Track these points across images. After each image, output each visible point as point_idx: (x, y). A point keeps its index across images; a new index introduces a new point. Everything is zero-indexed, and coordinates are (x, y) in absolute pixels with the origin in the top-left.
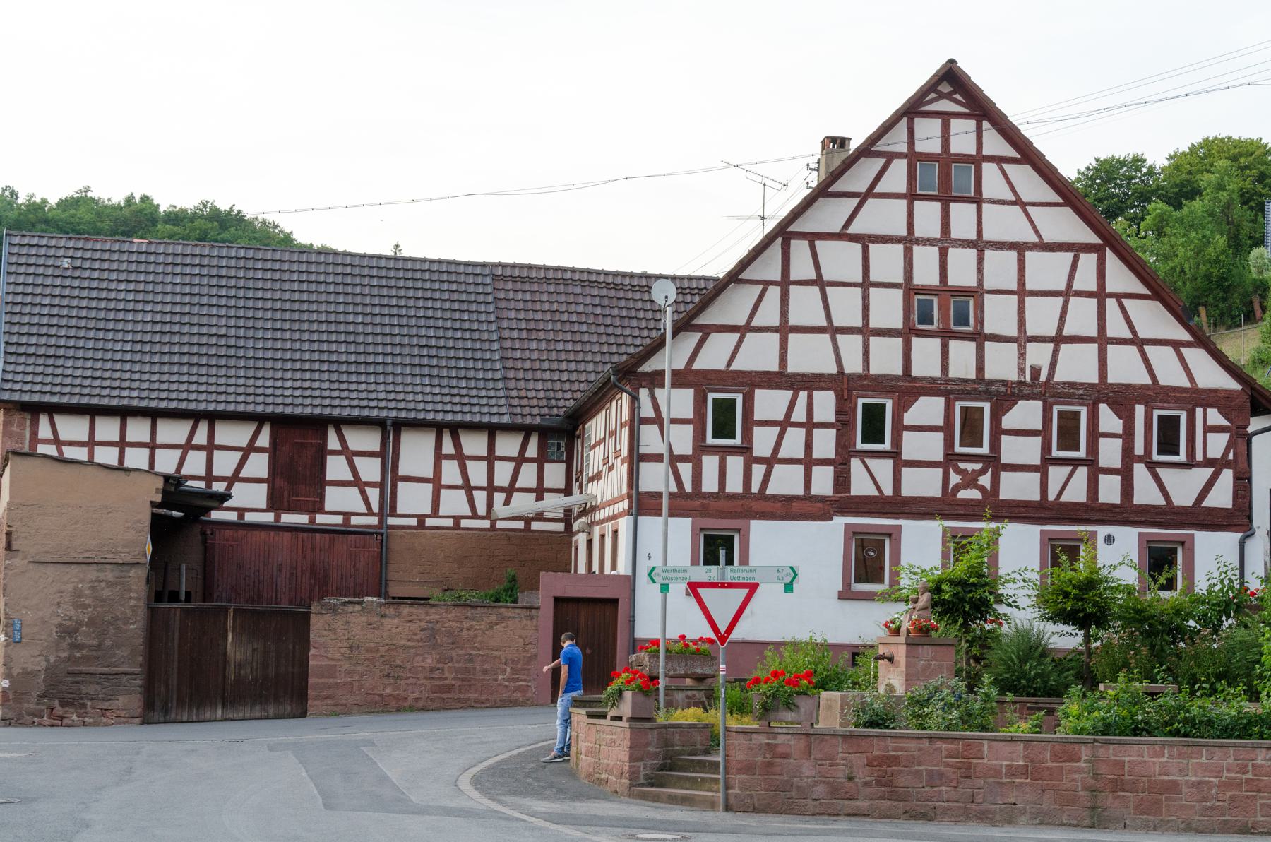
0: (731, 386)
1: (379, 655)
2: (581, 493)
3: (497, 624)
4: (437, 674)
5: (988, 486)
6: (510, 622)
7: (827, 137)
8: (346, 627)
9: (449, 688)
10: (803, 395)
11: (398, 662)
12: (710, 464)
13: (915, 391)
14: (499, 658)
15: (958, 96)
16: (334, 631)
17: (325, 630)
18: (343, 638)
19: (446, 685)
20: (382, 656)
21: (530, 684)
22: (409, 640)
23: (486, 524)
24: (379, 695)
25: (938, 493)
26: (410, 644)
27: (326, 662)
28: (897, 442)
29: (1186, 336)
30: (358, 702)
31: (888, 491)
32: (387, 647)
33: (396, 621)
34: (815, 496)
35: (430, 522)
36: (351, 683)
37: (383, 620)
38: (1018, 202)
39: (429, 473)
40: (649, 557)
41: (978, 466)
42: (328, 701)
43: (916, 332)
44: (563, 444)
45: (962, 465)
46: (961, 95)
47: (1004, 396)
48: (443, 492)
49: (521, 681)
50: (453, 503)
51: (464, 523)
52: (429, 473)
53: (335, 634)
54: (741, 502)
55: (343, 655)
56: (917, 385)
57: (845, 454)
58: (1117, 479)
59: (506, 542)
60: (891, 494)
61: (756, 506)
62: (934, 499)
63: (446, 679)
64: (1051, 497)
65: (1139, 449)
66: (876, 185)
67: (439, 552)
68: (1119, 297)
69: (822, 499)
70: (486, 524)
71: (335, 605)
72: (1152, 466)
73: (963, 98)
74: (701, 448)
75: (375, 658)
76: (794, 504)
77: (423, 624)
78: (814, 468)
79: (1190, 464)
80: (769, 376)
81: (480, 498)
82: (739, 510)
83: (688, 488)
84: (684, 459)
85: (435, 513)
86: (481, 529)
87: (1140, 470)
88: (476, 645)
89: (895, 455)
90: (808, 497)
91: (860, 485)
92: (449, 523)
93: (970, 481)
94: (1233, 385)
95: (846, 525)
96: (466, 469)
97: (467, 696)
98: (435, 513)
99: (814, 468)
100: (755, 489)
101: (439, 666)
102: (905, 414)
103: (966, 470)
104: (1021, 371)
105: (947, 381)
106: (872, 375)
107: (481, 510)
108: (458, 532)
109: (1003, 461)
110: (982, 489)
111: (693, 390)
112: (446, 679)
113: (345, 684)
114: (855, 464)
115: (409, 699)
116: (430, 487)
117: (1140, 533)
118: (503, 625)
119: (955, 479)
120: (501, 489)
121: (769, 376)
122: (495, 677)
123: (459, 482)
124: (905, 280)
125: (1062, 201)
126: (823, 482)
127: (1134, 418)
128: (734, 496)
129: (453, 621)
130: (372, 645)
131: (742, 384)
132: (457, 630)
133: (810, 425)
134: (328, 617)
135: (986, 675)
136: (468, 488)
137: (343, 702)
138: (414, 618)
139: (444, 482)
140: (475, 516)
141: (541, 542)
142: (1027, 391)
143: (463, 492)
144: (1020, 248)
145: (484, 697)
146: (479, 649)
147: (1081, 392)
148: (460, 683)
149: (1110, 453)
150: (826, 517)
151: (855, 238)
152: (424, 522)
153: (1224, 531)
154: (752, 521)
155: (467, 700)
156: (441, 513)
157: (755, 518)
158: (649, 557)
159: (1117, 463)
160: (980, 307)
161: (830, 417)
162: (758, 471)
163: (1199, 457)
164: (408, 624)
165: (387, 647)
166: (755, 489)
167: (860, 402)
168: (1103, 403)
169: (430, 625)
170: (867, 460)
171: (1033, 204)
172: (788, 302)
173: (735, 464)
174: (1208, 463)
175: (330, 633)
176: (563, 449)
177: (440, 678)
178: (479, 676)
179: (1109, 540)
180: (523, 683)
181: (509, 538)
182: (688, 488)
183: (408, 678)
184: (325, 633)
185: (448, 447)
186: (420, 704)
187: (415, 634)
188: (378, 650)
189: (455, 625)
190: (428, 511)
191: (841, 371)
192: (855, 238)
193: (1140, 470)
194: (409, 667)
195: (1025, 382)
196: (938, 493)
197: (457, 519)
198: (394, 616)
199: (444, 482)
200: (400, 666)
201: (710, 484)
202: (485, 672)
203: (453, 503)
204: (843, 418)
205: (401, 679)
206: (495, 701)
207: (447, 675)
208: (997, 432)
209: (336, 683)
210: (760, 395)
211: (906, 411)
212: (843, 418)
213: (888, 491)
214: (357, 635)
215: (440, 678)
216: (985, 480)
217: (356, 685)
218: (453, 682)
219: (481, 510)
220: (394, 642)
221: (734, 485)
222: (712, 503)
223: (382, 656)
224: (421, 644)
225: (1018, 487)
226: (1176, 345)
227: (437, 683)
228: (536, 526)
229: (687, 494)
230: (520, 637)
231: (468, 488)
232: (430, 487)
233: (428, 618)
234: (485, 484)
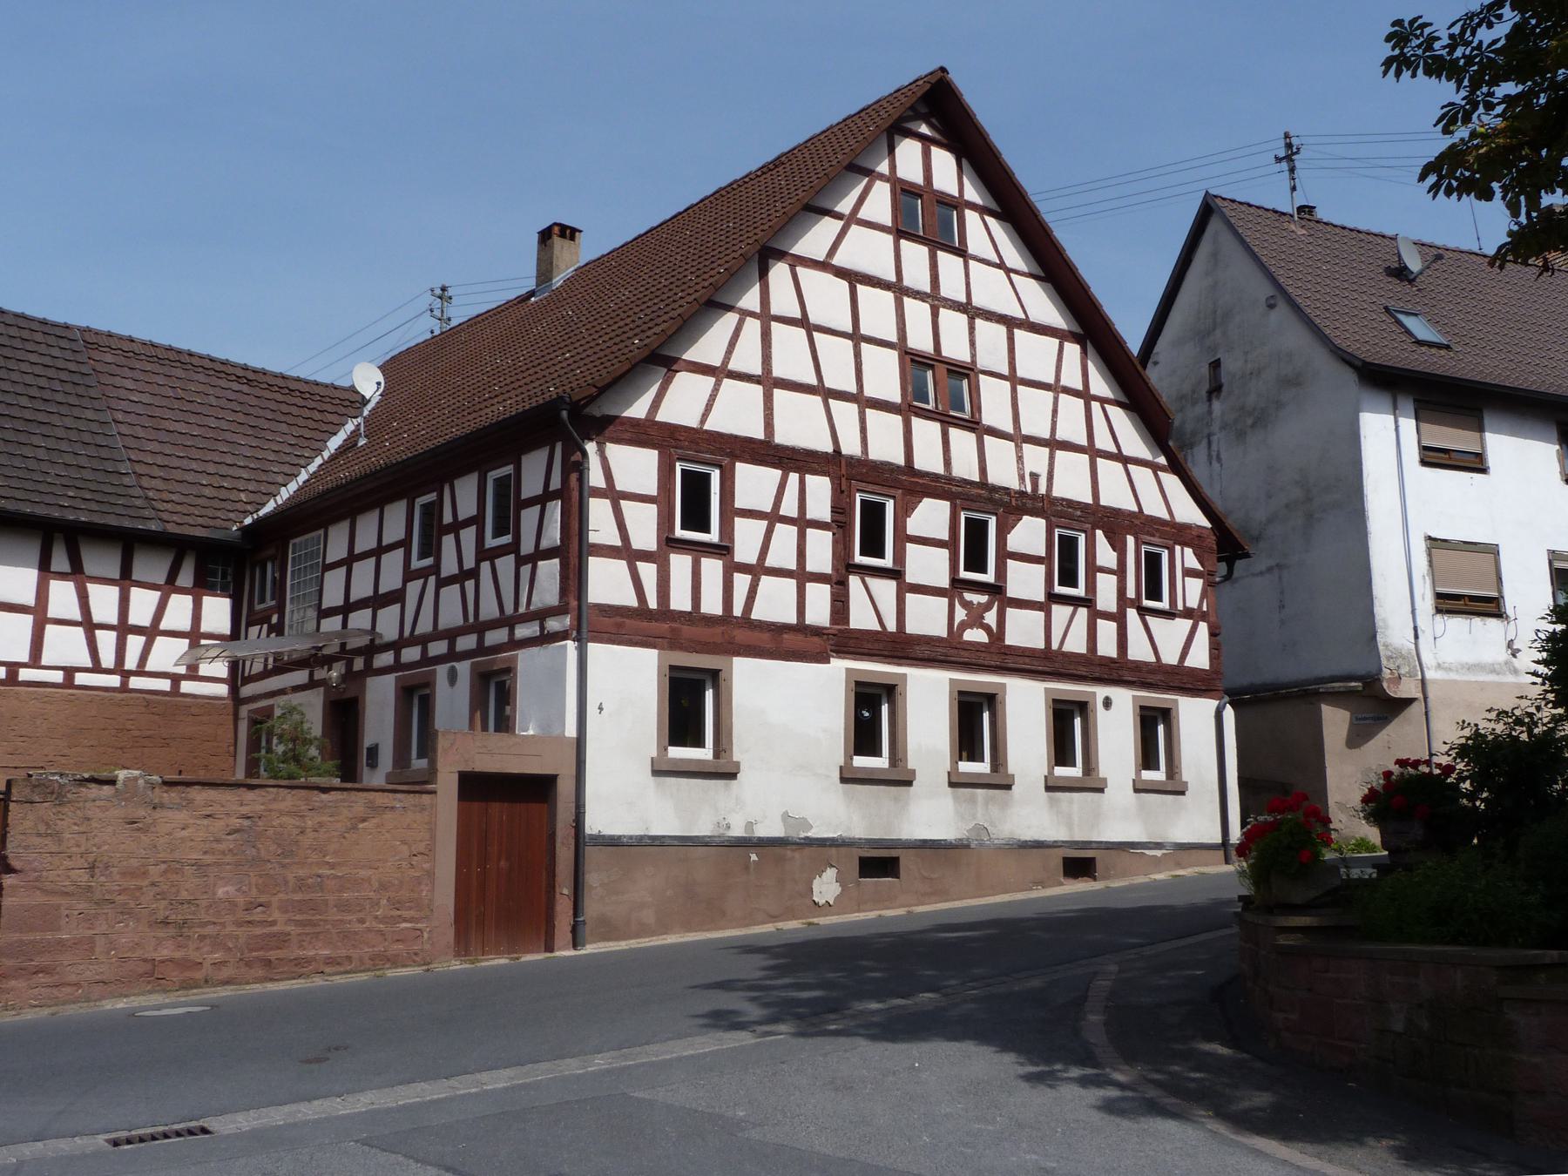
0: (706, 453)
1: (146, 882)
2: (246, 639)
3: (364, 820)
4: (257, 914)
5: (994, 626)
6: (388, 816)
7: (555, 224)
8: (82, 829)
9: (282, 940)
10: (794, 478)
11: (184, 895)
12: (680, 564)
13: (918, 489)
14: (369, 880)
15: (934, 120)
16: (57, 836)
17: (39, 835)
18: (74, 849)
19: (274, 935)
20: (153, 884)
21: (419, 926)
22: (205, 853)
23: (114, 681)
24: (145, 960)
25: (943, 632)
26: (208, 859)
27: (39, 898)
28: (900, 556)
29: (1162, 460)
30: (104, 977)
31: (891, 626)
32: (163, 867)
33: (181, 816)
34: (809, 626)
35: (25, 674)
36: (91, 941)
37: (158, 814)
38: (1001, 265)
39: (29, 599)
40: (601, 709)
41: (984, 599)
42: (41, 978)
43: (916, 410)
44: (230, 570)
45: (968, 596)
46: (937, 119)
47: (1014, 505)
48: (49, 629)
49: (405, 920)
50: (65, 646)
51: (81, 679)
52: (29, 599)
53: (60, 841)
54: (719, 630)
55: (74, 883)
56: (921, 481)
57: (844, 569)
58: (1113, 625)
59: (143, 710)
60: (895, 631)
61: (741, 636)
62: (939, 639)
63: (273, 923)
64: (1055, 646)
65: (1131, 593)
66: (859, 209)
67: (38, 722)
68: (1103, 401)
69: (817, 631)
70: (114, 681)
71: (61, 786)
72: (1143, 612)
73: (939, 123)
74: (670, 543)
75: (141, 888)
76: (785, 636)
77: (236, 822)
78: (807, 584)
79: (1169, 615)
80: (753, 446)
81: (106, 640)
82: (719, 640)
83: (653, 603)
84: (646, 556)
85: (35, 661)
86: (106, 689)
87: (1132, 614)
88: (327, 859)
89: (896, 574)
90: (801, 628)
91: (861, 618)
92: (58, 677)
93: (976, 620)
94: (1203, 521)
95: (848, 671)
96: (87, 597)
97: (312, 953)
98: (35, 661)
99: (807, 584)
100: (738, 611)
101: (262, 899)
102: (908, 519)
103: (971, 602)
104: (1022, 478)
105: (949, 479)
106: (873, 461)
107: (107, 660)
108: (70, 691)
109: (1010, 594)
110: (987, 628)
111: (656, 452)
112: (273, 923)
113: (77, 943)
114: (854, 582)
115: (207, 965)
116: (28, 620)
117: (1133, 696)
118: (375, 821)
119: (961, 614)
120: (138, 630)
121: (753, 446)
122: (361, 915)
123: (76, 615)
124: (899, 340)
125: (1043, 275)
126: (819, 609)
127: (1126, 551)
128: (710, 620)
129: (289, 813)
130: (134, 863)
131: (721, 452)
132: (296, 831)
133: (803, 523)
134: (46, 810)
135: (1374, 875)
136: (89, 625)
137: (73, 978)
138: (215, 809)
139: (50, 614)
140: (97, 668)
141: (193, 710)
142: (1029, 504)
143: (80, 630)
144: (1009, 323)
145: (343, 952)
146: (332, 866)
147: (1079, 513)
148: (299, 930)
149: (1106, 589)
150: (822, 658)
151: (841, 273)
152: (16, 674)
153: (1200, 696)
154: (734, 658)
155: (309, 961)
156: (44, 662)
157: (739, 655)
158: (601, 709)
159: (1113, 608)
160: (975, 391)
161: (826, 515)
162: (742, 582)
163: (1180, 606)
164: (205, 822)
165: (163, 867)
166: (738, 611)
167: (858, 498)
168: (1099, 529)
169: (246, 823)
170: (867, 579)
171: (1017, 272)
172: (770, 343)
173: (712, 568)
174: (1188, 613)
175: (47, 841)
176: (229, 578)
177: (263, 923)
178: (334, 915)
179: (1107, 703)
180: (409, 925)
181: (148, 703)
182: (653, 603)
183: (204, 924)
184: (37, 841)
185: (60, 562)
186: (226, 973)
187: (218, 841)
188: (145, 873)
189: (289, 821)
190: (24, 657)
191: (837, 451)
192: (841, 273)
193: (1132, 614)
194: (204, 903)
195: (1026, 493)
196: (943, 632)
197: (69, 672)
198: (180, 807)
199: (50, 614)
200: (189, 902)
201: (680, 600)
202: (344, 907)
203: (65, 646)
204: (841, 518)
205: (190, 928)
206: (361, 960)
207: (276, 915)
208: (1004, 555)
209: (60, 942)
210: (744, 471)
211: (910, 517)
212: (841, 518)
213: (891, 626)
214: (105, 843)
215: (263, 923)
216: (991, 618)
217: (100, 943)
218: (288, 929)
219: (107, 660)
220: (177, 855)
221: (712, 604)
222: (687, 631)
223: (153, 884)
224: (228, 859)
225: (1023, 630)
226: (1155, 468)
227: (258, 931)
228: (187, 687)
229: (651, 611)
230: (404, 842)
231: (89, 625)
232: (28, 620)
233: (244, 810)
234: (114, 620)
